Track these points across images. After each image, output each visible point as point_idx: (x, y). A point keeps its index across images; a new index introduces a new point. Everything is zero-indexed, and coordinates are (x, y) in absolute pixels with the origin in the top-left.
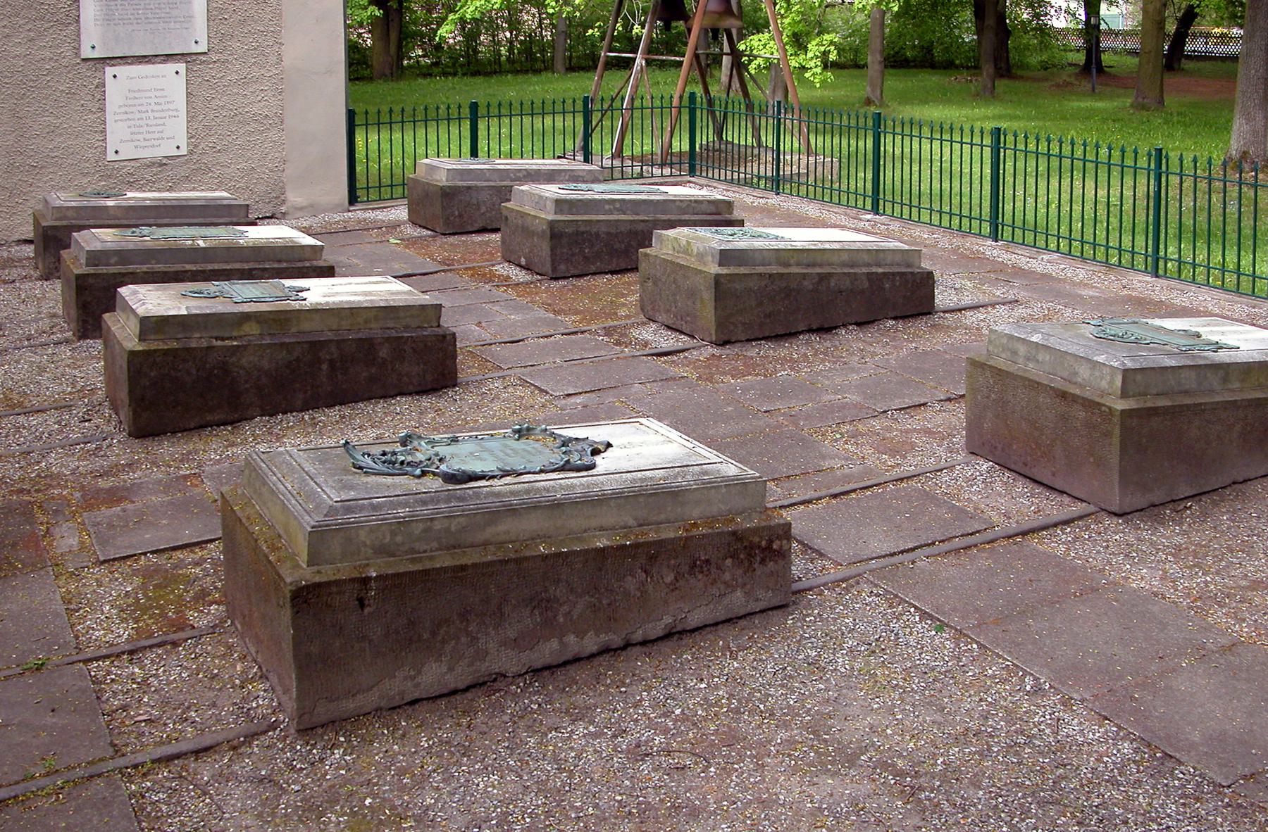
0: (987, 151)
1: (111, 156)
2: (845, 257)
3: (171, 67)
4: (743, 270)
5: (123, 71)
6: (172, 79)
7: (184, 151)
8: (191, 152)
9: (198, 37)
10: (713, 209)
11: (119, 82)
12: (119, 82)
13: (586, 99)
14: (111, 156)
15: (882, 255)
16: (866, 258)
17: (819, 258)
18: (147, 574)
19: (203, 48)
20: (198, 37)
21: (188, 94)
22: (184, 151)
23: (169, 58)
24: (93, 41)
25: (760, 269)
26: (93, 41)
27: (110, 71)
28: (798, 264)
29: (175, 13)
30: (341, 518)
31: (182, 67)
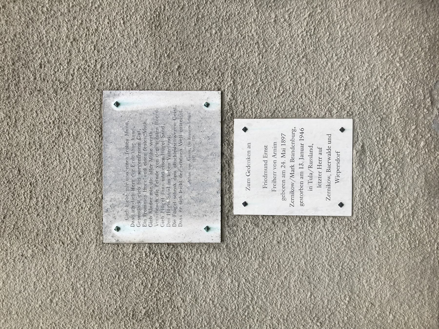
1: (347, 211)
3: (239, 138)
5: (239, 194)
6: (254, 136)
7: (348, 123)
12: (253, 198)
14: (347, 211)
19: (214, 98)
21: (273, 116)
22: (348, 123)
24: (199, 228)
27: (238, 210)
29: (169, 131)
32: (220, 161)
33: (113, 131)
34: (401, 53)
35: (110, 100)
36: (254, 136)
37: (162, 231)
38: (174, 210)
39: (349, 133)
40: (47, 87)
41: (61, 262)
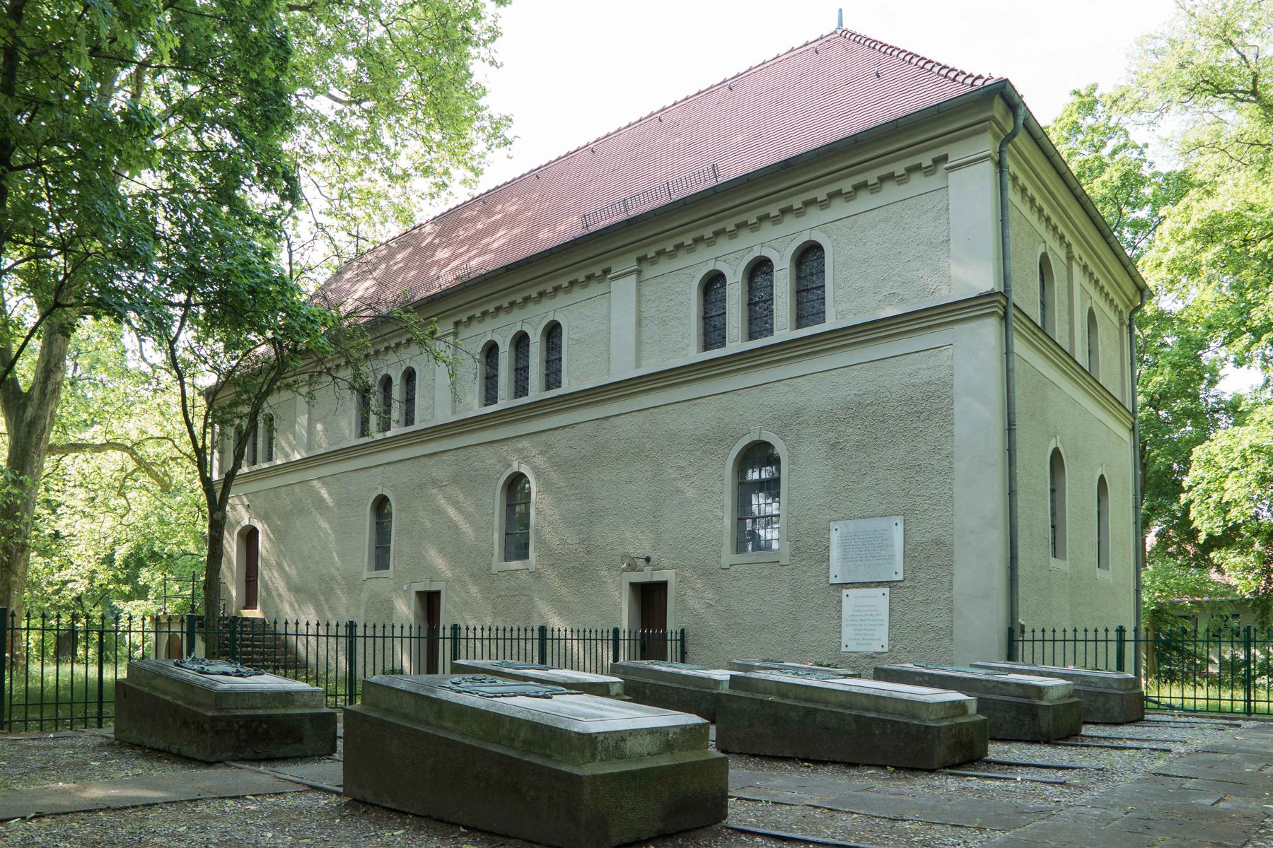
0: (536, 642)
1: (844, 649)
2: (843, 698)
3: (881, 590)
4: (743, 694)
5: (853, 592)
6: (880, 598)
7: (886, 649)
8: (891, 651)
9: (896, 570)
10: (1021, 692)
11: (851, 599)
12: (851, 599)
13: (682, 631)
14: (844, 649)
15: (882, 702)
16: (865, 702)
17: (816, 696)
18: (28, 396)
19: (900, 577)
20: (896, 570)
21: (891, 610)
22: (886, 649)
23: (879, 584)
24: (837, 572)
25: (760, 696)
26: (837, 572)
27: (845, 592)
28: (796, 698)
29: (883, 553)
30: (274, 593)
31: (887, 590)
32: (633, 311)
33: (880, 524)
34: (251, 132)
35: (900, 520)
36: (880, 598)
37: (835, 553)
38: (845, 558)
39: (880, 650)
40: (906, 485)
41: (821, 501)
